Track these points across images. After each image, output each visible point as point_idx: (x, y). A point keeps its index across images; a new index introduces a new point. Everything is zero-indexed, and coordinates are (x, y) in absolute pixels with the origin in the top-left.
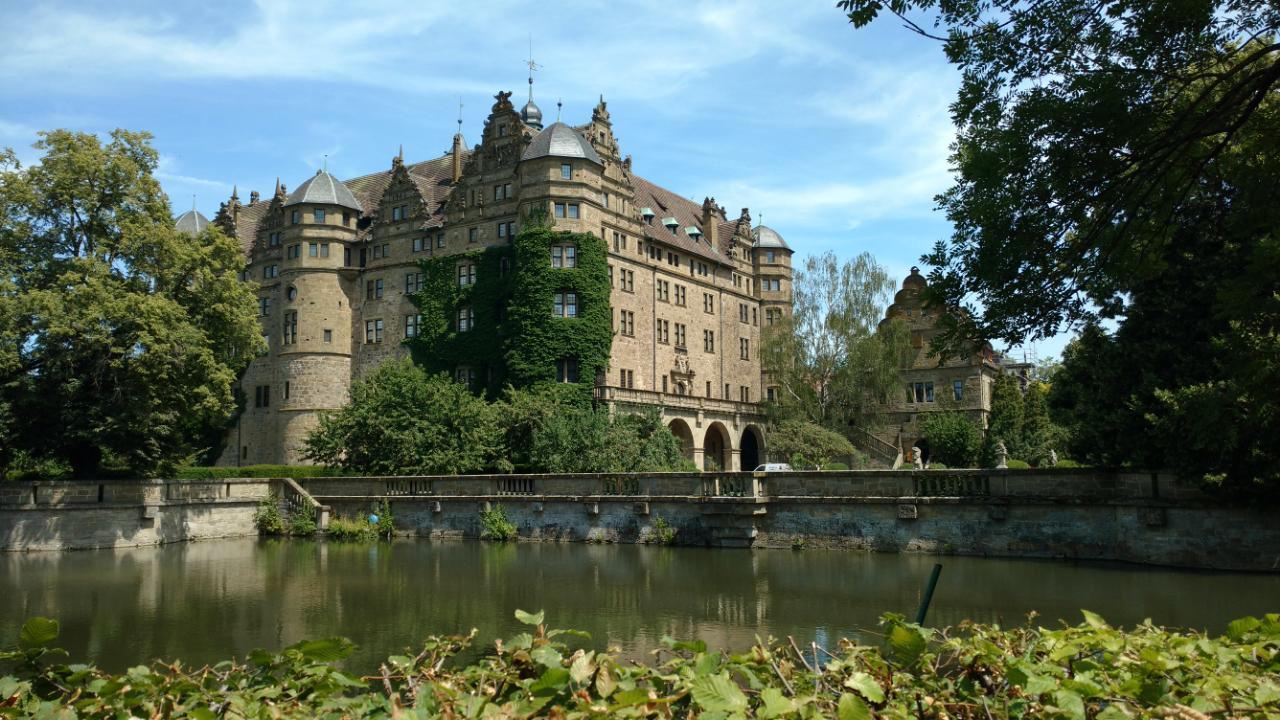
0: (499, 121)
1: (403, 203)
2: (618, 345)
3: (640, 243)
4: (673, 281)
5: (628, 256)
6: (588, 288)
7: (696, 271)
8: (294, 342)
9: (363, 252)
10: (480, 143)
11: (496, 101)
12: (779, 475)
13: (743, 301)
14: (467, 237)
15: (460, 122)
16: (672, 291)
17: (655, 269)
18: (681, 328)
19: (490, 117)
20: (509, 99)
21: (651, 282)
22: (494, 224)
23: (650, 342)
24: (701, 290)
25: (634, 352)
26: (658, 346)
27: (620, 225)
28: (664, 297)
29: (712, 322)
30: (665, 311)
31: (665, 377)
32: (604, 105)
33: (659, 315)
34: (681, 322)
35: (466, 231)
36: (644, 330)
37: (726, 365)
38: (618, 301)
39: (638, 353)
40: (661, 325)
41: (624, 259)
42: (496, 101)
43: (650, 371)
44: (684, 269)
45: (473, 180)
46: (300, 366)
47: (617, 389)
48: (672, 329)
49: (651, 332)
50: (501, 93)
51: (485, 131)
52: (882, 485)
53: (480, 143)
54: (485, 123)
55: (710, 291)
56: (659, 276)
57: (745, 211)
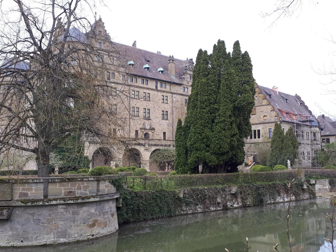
44: (152, 85)
55: (165, 94)
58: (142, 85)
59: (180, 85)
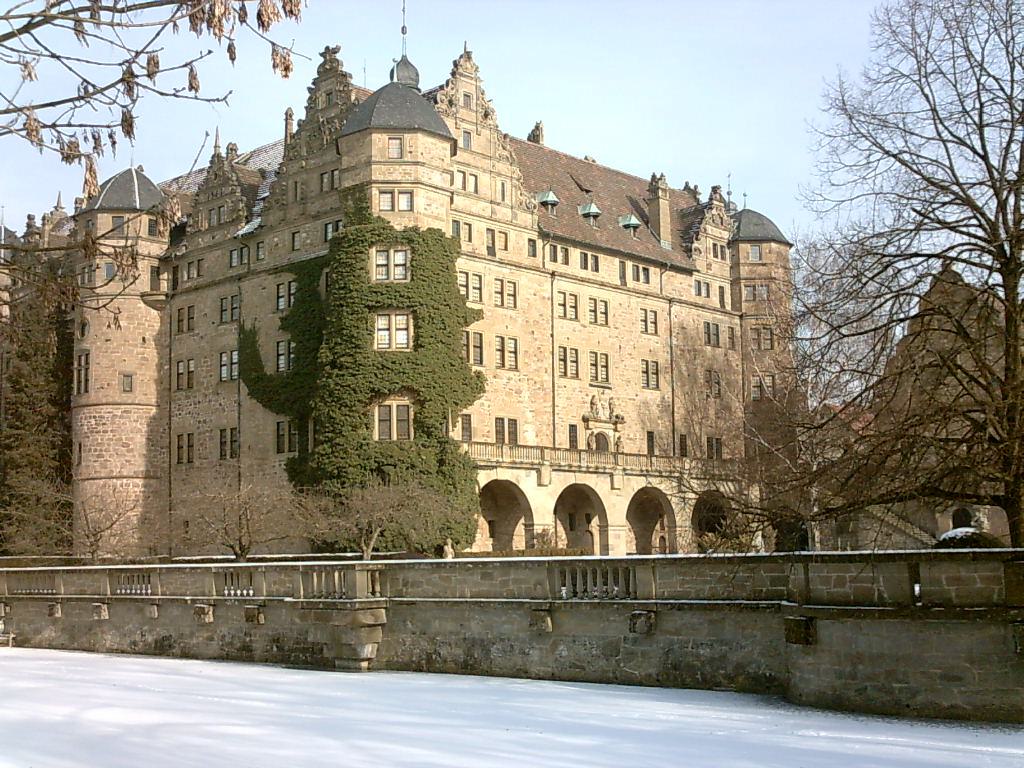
0: (325, 86)
1: (220, 203)
2: (498, 382)
3: (532, 242)
5: (515, 259)
6: (437, 305)
8: (86, 391)
9: (175, 270)
10: (304, 118)
11: (322, 60)
12: (658, 559)
14: (288, 243)
15: (745, 195)
16: (585, 307)
18: (601, 362)
20: (338, 56)
21: (548, 295)
22: (319, 223)
23: (547, 378)
24: (635, 300)
25: (519, 392)
26: (560, 382)
27: (499, 216)
28: (570, 312)
30: (568, 333)
31: (573, 428)
32: (467, 55)
33: (560, 341)
35: (287, 236)
36: (537, 366)
38: (491, 327)
39: (526, 395)
40: (567, 358)
42: (322, 60)
43: (548, 418)
44: (609, 267)
45: (295, 167)
46: (93, 421)
47: (547, 448)
49: (547, 363)
50: (327, 48)
52: (516, 581)
53: (304, 118)
54: (309, 89)
58: (583, 274)
59: (689, 272)
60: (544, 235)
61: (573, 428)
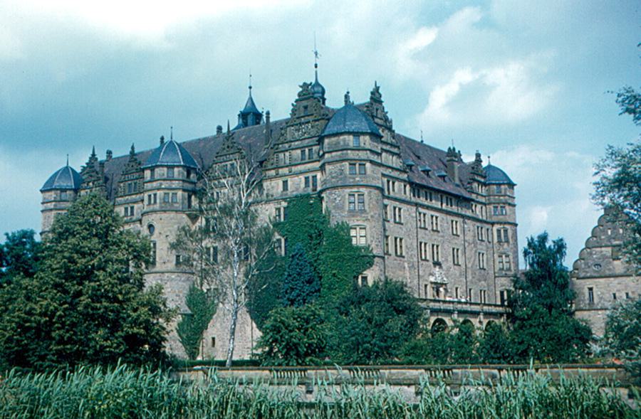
3: (405, 186)
4: (429, 213)
5: (398, 196)
7: (444, 205)
11: (301, 89)
13: (479, 224)
15: (250, 88)
17: (417, 205)
19: (296, 101)
24: (450, 218)
26: (421, 262)
29: (458, 243)
34: (399, 236)
35: (280, 183)
37: (469, 272)
41: (396, 199)
48: (429, 249)
51: (293, 111)
55: (455, 219)
56: (421, 210)
57: (478, 155)
60: (411, 184)
61: (426, 286)
